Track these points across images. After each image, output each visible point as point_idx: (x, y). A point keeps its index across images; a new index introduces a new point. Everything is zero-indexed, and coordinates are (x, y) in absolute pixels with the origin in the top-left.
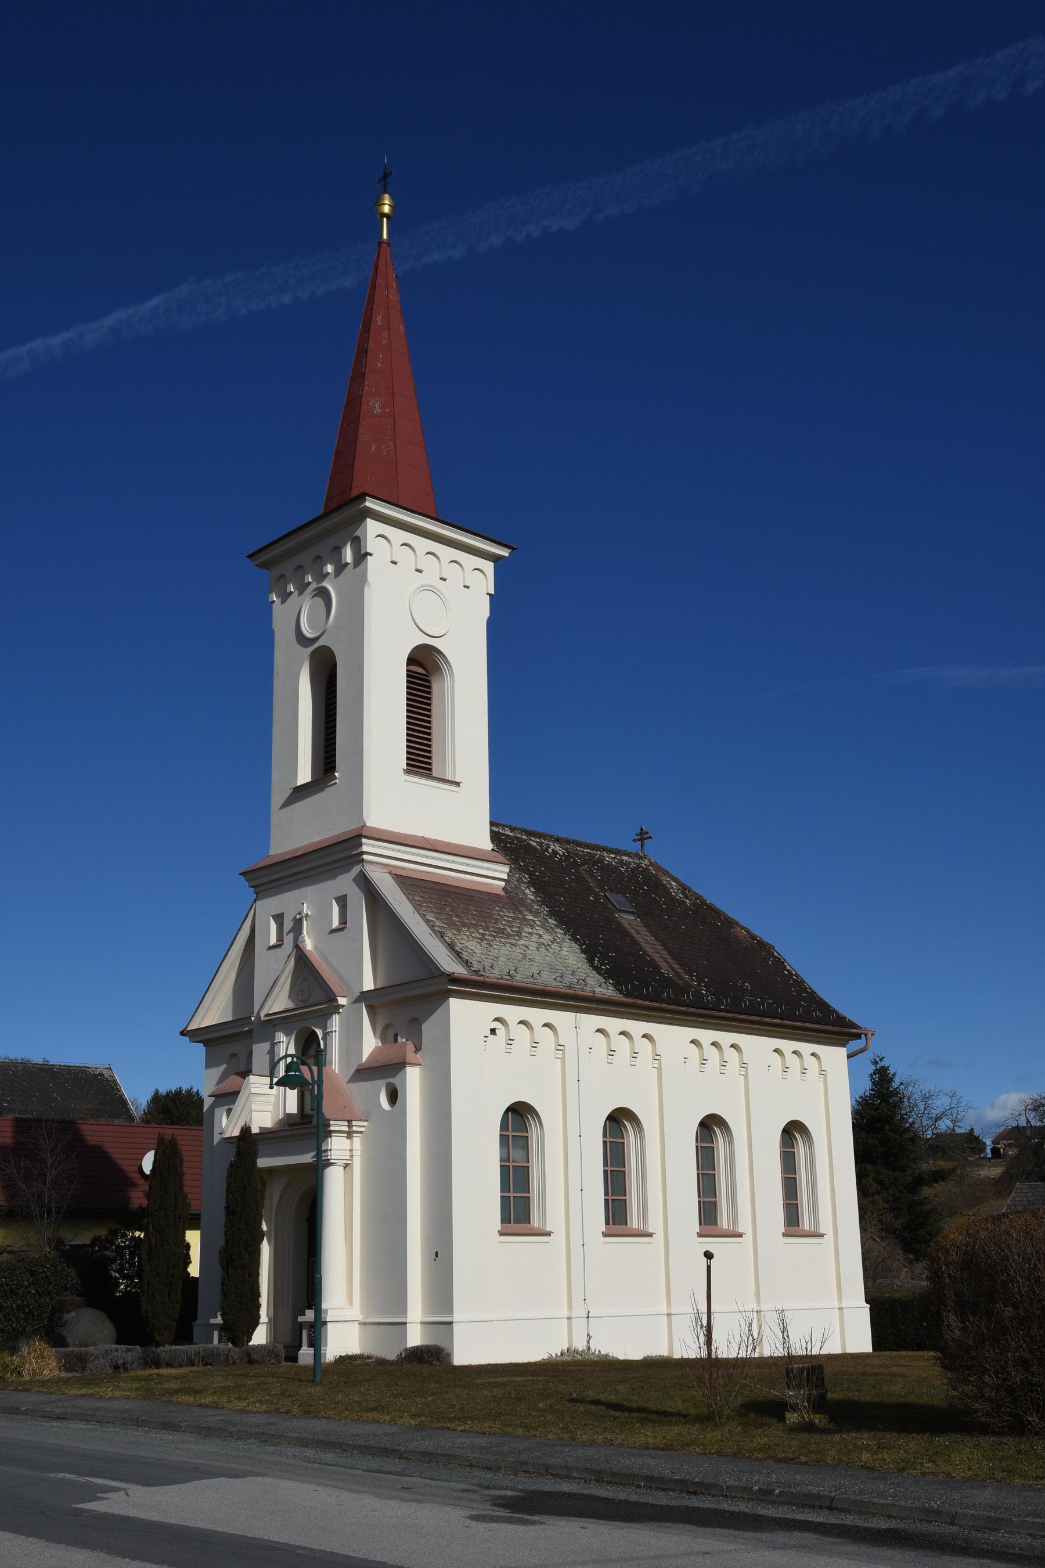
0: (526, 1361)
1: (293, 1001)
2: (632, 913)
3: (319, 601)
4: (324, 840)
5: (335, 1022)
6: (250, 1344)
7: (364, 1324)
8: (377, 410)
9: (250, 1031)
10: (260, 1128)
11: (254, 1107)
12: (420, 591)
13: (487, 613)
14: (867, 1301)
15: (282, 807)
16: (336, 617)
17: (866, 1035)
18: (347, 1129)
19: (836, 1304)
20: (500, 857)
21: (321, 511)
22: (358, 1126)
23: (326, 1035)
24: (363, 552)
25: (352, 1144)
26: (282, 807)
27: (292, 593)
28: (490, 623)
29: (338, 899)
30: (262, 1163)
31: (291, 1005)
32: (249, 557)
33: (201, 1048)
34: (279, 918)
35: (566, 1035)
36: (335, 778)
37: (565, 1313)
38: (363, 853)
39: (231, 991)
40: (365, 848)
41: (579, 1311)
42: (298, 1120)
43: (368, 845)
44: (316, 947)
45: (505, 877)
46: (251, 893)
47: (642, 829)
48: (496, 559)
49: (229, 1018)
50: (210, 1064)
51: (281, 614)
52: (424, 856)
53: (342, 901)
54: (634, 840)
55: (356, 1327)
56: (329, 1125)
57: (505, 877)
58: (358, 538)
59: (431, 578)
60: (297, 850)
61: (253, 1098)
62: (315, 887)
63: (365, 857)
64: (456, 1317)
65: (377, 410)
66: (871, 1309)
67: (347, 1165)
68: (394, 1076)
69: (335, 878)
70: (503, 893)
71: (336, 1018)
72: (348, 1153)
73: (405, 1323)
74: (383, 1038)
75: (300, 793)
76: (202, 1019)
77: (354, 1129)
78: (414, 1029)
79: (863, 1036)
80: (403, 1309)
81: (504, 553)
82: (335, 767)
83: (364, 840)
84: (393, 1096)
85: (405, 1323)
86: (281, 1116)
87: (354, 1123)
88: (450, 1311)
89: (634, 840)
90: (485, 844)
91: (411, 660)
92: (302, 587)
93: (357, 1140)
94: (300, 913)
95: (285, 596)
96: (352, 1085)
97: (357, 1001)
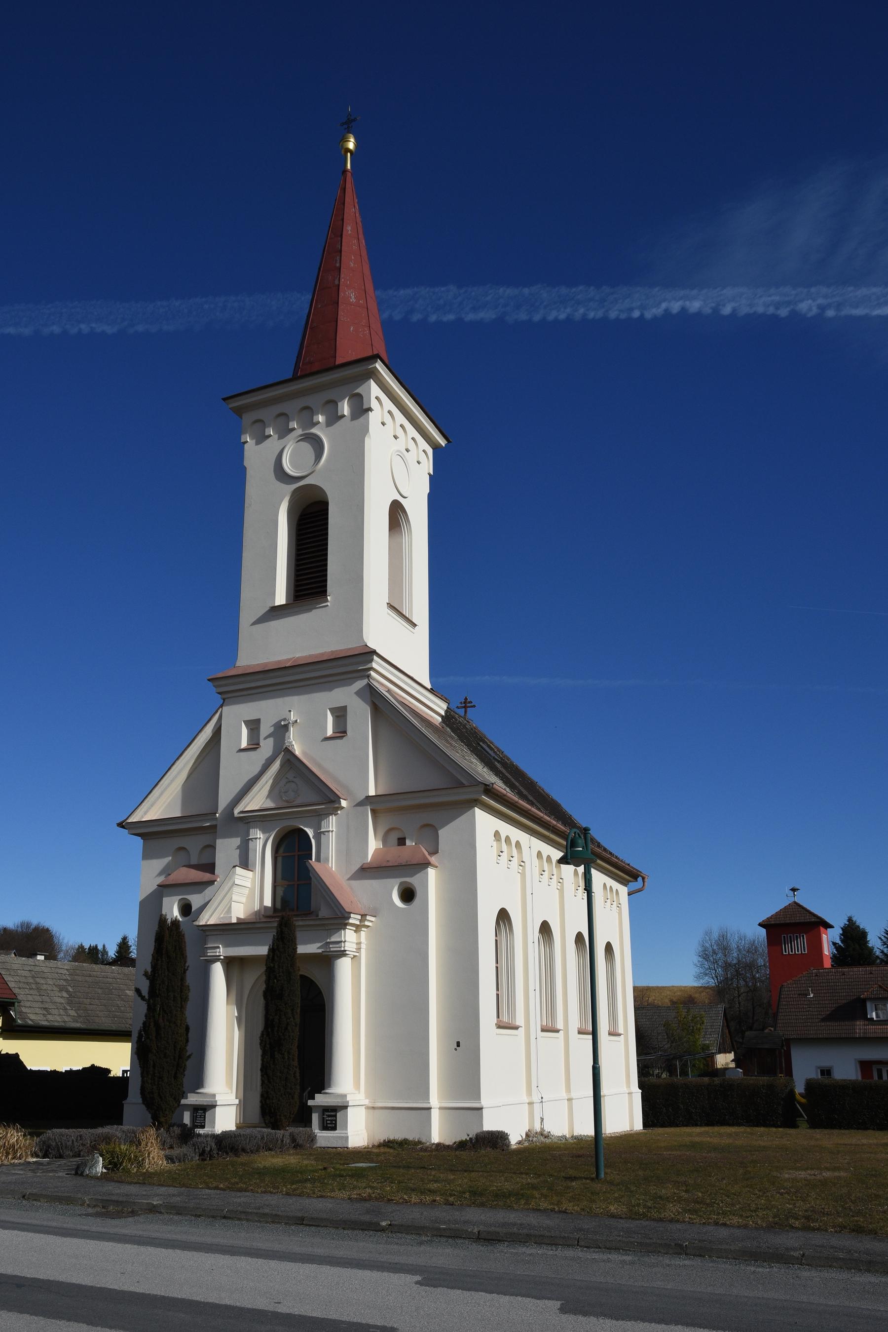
1: (273, 801)
3: (306, 447)
4: (322, 654)
5: (332, 823)
7: (373, 1108)
8: (353, 300)
9: (213, 828)
10: (238, 918)
11: (234, 898)
12: (392, 456)
15: (254, 623)
16: (326, 460)
17: (643, 879)
18: (358, 923)
19: (565, 1095)
21: (289, 375)
22: (370, 921)
23: (318, 835)
24: (365, 407)
25: (359, 937)
26: (254, 623)
27: (270, 436)
28: (431, 497)
29: (247, 723)
30: (302, 949)
31: (270, 804)
32: (224, 399)
33: (139, 841)
34: (254, 726)
36: (327, 601)
37: (526, 1100)
38: (372, 669)
39: (180, 787)
40: (374, 665)
41: (536, 1098)
42: (271, 913)
43: (377, 664)
44: (304, 753)
46: (219, 699)
47: (466, 699)
48: (436, 448)
49: (178, 814)
50: (147, 855)
51: (257, 455)
53: (340, 714)
55: (363, 1110)
56: (349, 918)
58: (359, 396)
59: (401, 444)
60: (266, 664)
61: (235, 889)
62: (304, 698)
63: (372, 673)
64: (485, 1101)
65: (353, 300)
67: (355, 956)
68: (412, 875)
69: (330, 690)
71: (333, 819)
72: (355, 946)
73: (481, 1109)
74: (385, 841)
75: (276, 612)
76: (145, 813)
77: (367, 923)
78: (430, 834)
79: (640, 879)
80: (426, 1095)
81: (443, 442)
82: (326, 591)
83: (375, 658)
84: (408, 895)
85: (481, 1109)
86: (257, 907)
87: (368, 918)
88: (478, 1097)
92: (285, 432)
93: (363, 933)
94: (284, 720)
95: (262, 438)
96: (353, 882)
97: (361, 804)
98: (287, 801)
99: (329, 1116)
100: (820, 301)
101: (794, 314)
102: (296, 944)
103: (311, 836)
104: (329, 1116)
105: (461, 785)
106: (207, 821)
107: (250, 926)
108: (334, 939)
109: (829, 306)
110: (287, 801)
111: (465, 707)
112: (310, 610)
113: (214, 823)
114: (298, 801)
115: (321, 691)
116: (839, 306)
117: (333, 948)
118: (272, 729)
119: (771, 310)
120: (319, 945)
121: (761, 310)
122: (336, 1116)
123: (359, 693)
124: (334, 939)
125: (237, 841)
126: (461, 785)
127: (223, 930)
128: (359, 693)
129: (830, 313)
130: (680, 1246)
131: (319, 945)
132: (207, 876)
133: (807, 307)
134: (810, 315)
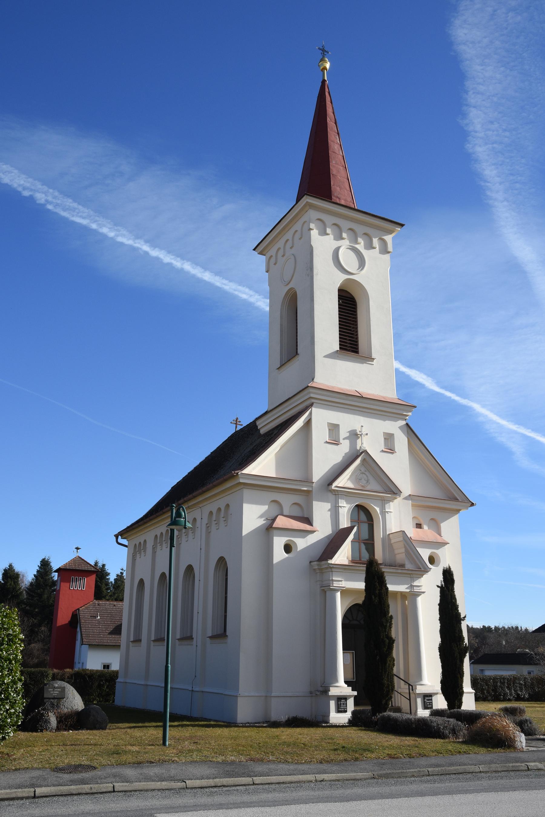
9: (308, 493)
34: (334, 428)
47: (237, 419)
69: (385, 420)
98: (363, 486)
99: (428, 700)
100: (50, 199)
101: (31, 198)
102: (386, 584)
103: (379, 512)
104: (428, 700)
105: (456, 499)
106: (306, 486)
107: (341, 567)
108: (415, 583)
109: (51, 203)
110: (363, 486)
111: (236, 424)
112: (363, 363)
113: (310, 489)
114: (368, 488)
115: (361, 416)
116: (57, 205)
117: (416, 590)
118: (348, 434)
119: (20, 189)
120: (407, 586)
121: (15, 185)
122: (431, 700)
123: (400, 428)
124: (415, 583)
125: (328, 506)
126: (456, 499)
127: (345, 569)
128: (400, 428)
129: (50, 207)
130: (117, 754)
131: (407, 586)
132: (307, 527)
133: (40, 198)
134: (38, 202)
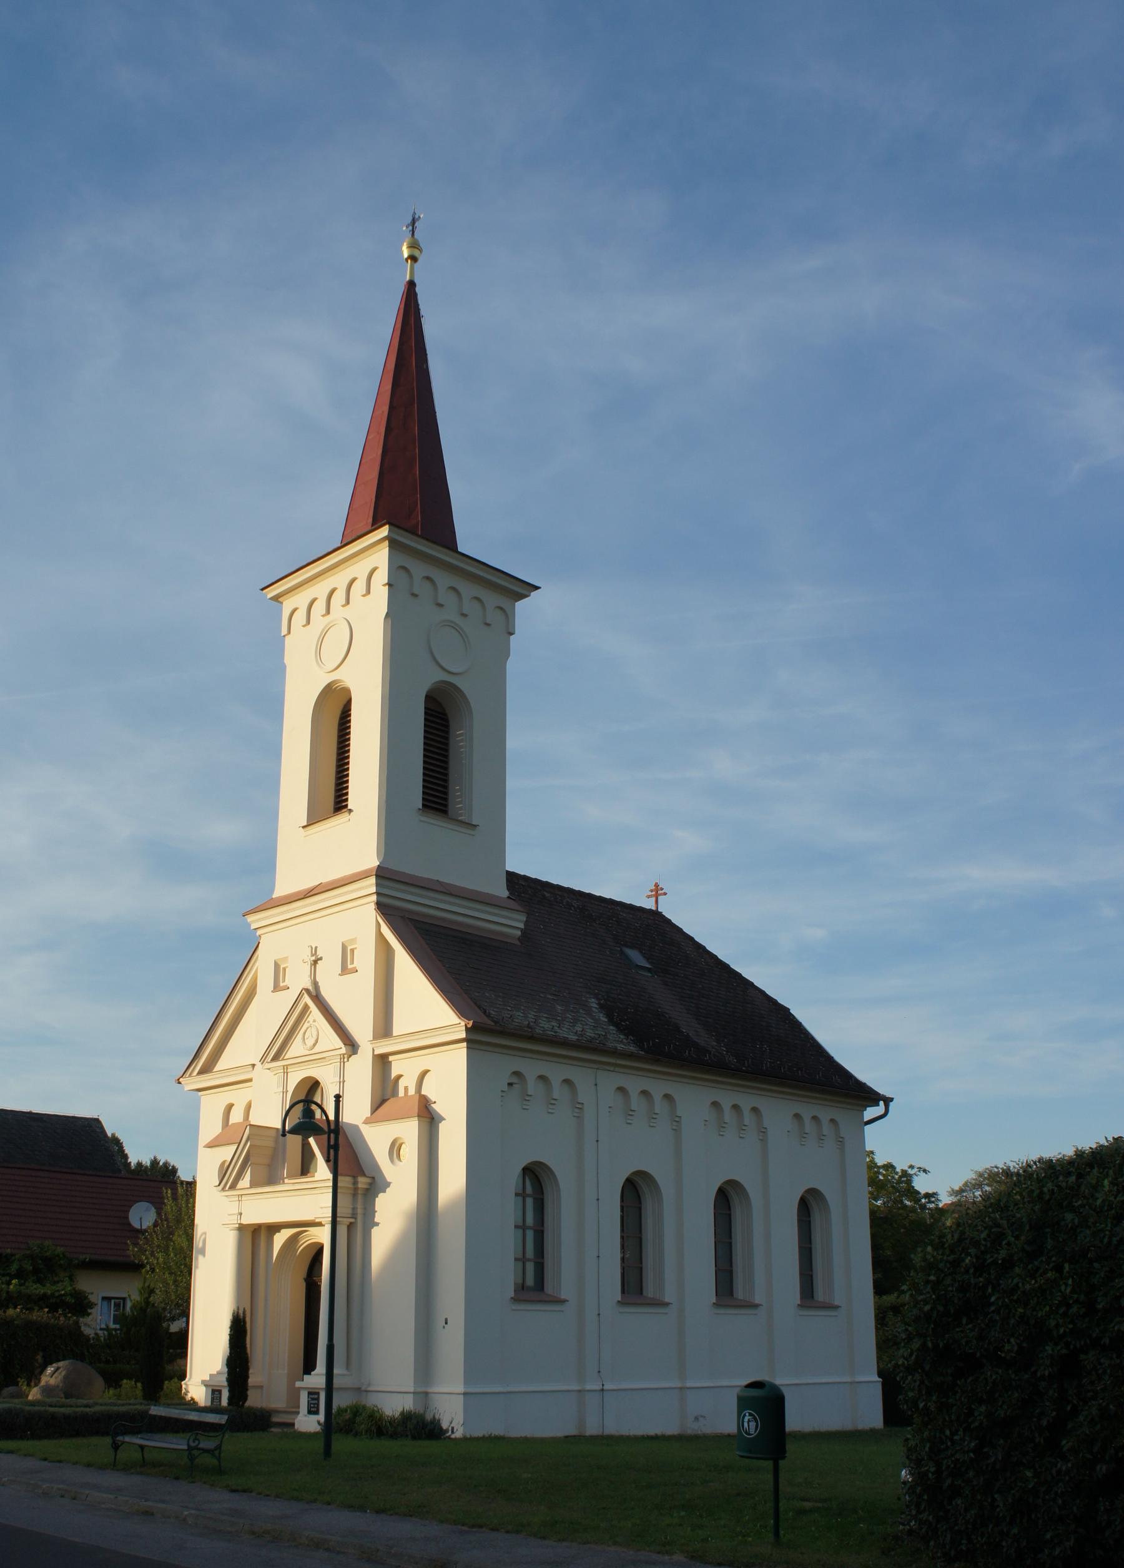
0: (437, 409)
2: (649, 970)
6: (247, 1404)
13: (510, 665)
14: (880, 1375)
20: (512, 904)
35: (585, 1094)
45: (522, 926)
52: (321, 901)
54: (649, 897)
57: (522, 926)
66: (883, 1384)
70: (518, 943)
89: (649, 897)
90: (504, 893)
91: (430, 699)
